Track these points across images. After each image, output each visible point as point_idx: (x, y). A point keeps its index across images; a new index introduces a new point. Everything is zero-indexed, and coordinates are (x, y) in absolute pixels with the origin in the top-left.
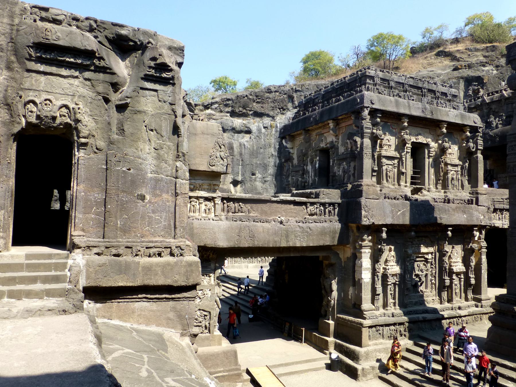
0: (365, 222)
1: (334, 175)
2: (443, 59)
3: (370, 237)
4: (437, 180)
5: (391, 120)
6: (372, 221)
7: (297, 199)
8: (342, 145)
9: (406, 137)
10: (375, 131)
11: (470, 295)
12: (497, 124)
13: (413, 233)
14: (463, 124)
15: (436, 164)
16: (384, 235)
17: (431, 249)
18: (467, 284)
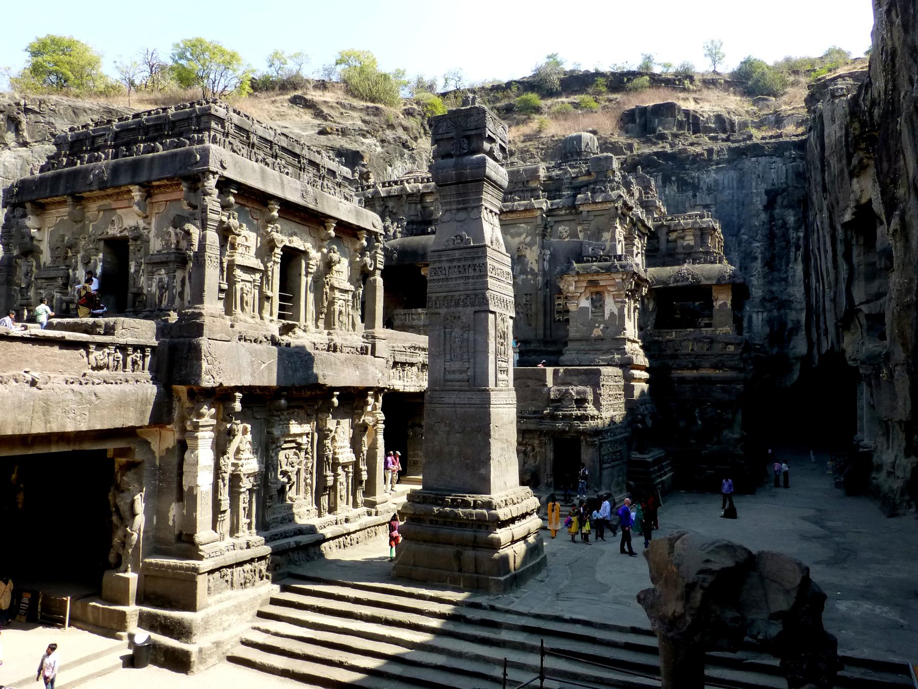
0: (207, 382)
1: (138, 294)
2: (302, 110)
3: (213, 410)
4: (318, 313)
5: (253, 200)
6: (219, 380)
7: (69, 335)
8: (157, 236)
9: (277, 236)
10: (225, 219)
11: (360, 498)
12: (395, 231)
13: (283, 401)
14: (358, 226)
15: (318, 285)
16: (238, 406)
17: (307, 428)
18: (357, 481)
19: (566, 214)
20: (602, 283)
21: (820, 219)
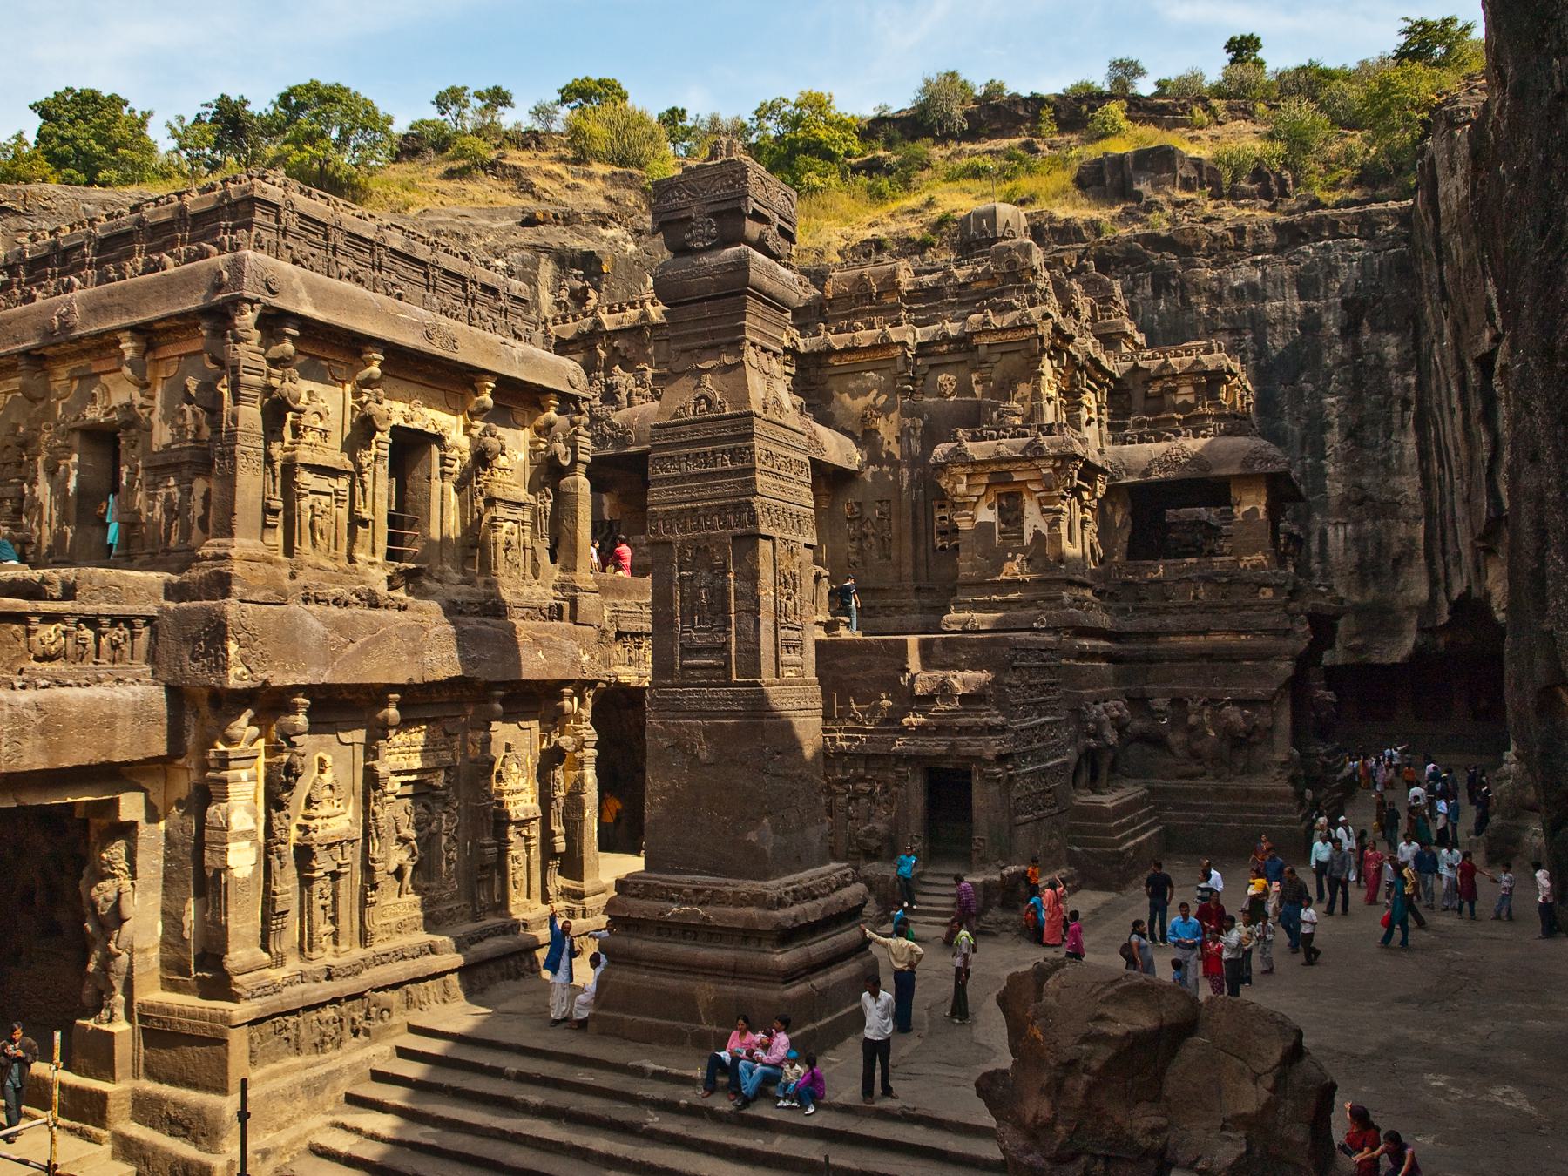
5: (331, 348)
8: (165, 419)
10: (275, 382)
14: (540, 386)
19: (949, 352)
21: (1442, 350)
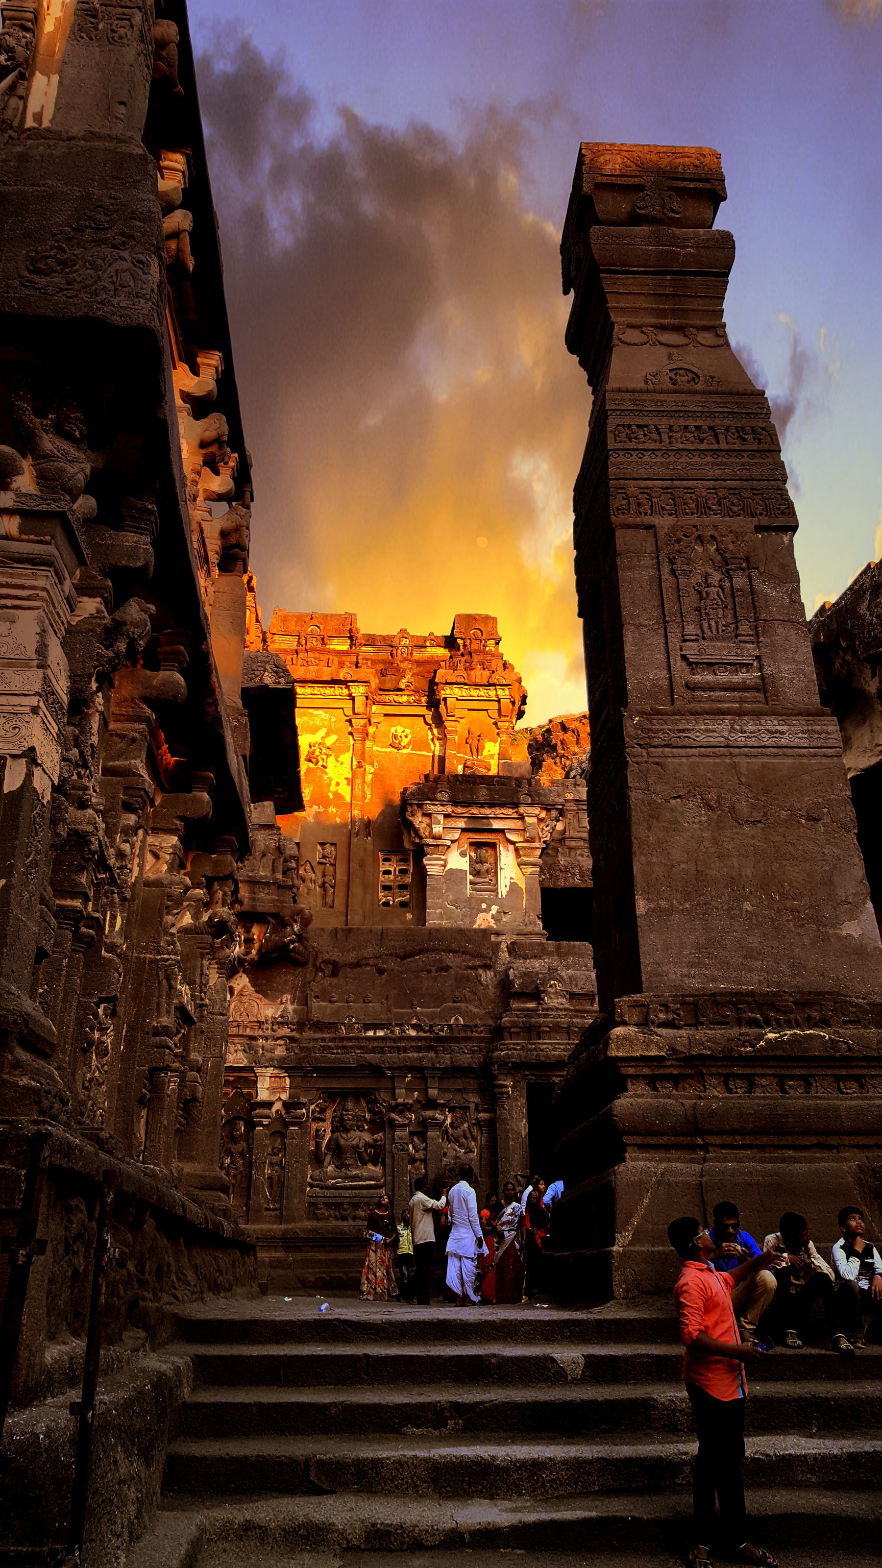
20: (496, 825)
